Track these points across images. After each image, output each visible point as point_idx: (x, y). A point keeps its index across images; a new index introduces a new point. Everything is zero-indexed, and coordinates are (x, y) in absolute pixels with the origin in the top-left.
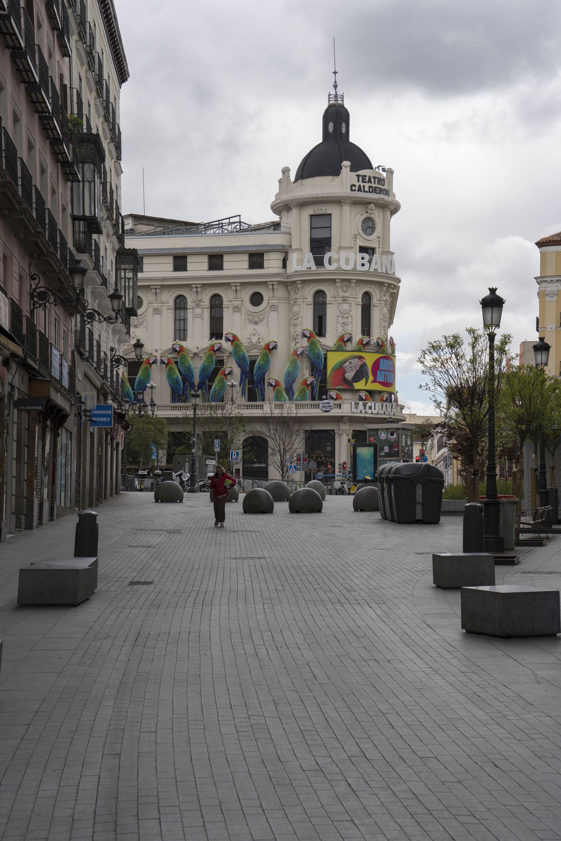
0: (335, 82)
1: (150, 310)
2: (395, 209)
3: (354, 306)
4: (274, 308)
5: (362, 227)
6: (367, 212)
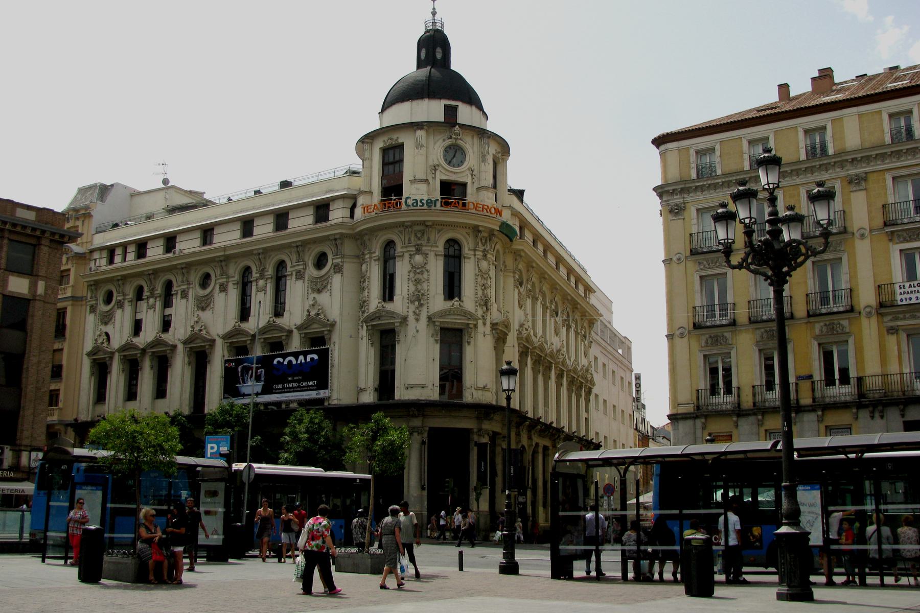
0: (434, 9)
1: (218, 287)
2: (660, 191)
3: (431, 256)
4: (338, 269)
5: (445, 156)
6: (451, 137)
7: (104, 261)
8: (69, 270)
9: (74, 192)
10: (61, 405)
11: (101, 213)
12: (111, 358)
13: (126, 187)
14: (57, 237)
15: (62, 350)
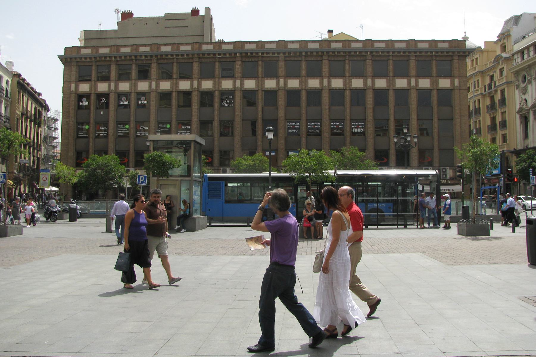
7: (519, 59)
8: (503, 68)
9: (502, 24)
10: (508, 142)
11: (516, 32)
12: (529, 113)
13: (530, 14)
14: (461, 54)
15: (505, 112)
